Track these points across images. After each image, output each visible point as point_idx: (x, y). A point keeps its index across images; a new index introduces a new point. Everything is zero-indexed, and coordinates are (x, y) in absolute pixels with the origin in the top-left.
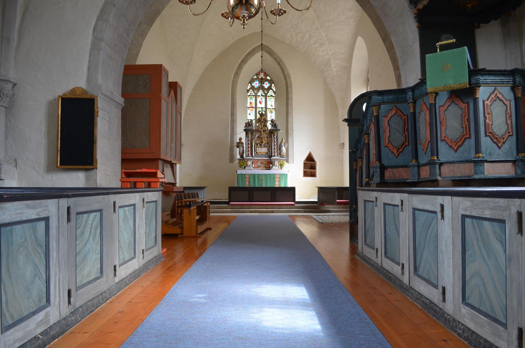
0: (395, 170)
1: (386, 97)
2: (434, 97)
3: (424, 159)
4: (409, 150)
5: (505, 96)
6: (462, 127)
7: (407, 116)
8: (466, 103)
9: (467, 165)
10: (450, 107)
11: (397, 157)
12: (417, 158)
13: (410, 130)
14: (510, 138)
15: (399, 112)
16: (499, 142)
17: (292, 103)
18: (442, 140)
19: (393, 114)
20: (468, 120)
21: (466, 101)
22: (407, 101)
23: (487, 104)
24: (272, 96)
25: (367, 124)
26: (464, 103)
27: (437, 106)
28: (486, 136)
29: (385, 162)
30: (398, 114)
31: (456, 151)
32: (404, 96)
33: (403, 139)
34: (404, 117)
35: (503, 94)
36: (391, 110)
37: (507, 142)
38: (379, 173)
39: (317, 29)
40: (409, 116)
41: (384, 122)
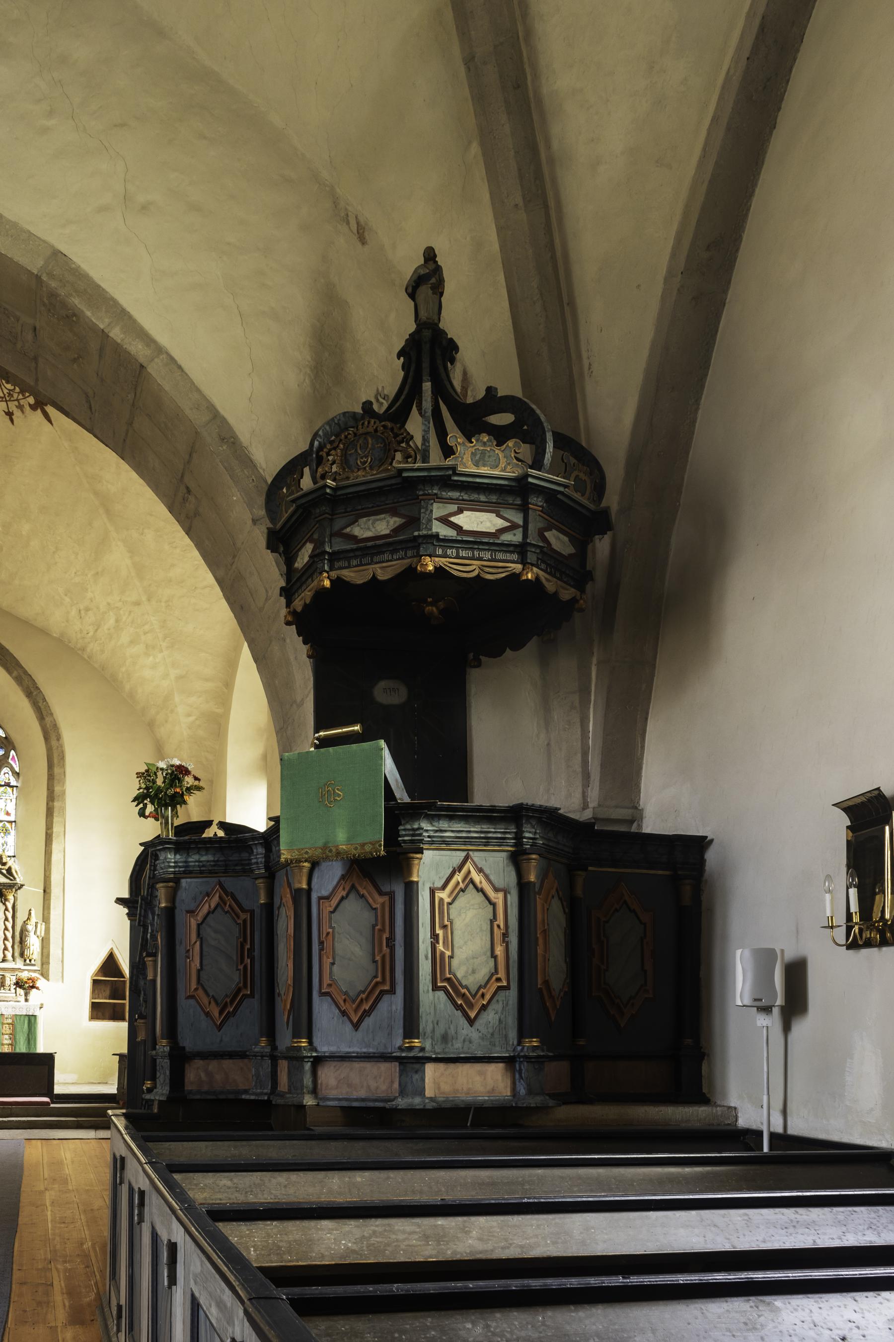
0: (213, 1065)
1: (196, 857)
2: (305, 871)
3: (285, 1040)
4: (252, 1009)
5: (492, 878)
6: (375, 962)
7: (252, 912)
8: (386, 894)
9: (384, 1066)
10: (345, 903)
11: (220, 1027)
12: (270, 1032)
13: (256, 953)
14: (502, 995)
15: (229, 901)
16: (471, 1006)
17: (63, 809)
18: (322, 994)
19: (213, 906)
20: (391, 941)
21: (386, 888)
22: (252, 871)
23: (441, 900)
24: (8, 785)
25: (152, 925)
26: (381, 893)
27: (314, 896)
28: (435, 988)
29: (187, 1042)
30: (227, 908)
31: (356, 1026)
32: (245, 855)
33: (236, 977)
34: (243, 916)
35: (487, 871)
36: (208, 895)
37: (494, 1006)
38: (168, 1073)
39: (138, 603)
40: (257, 911)
41: (187, 928)
